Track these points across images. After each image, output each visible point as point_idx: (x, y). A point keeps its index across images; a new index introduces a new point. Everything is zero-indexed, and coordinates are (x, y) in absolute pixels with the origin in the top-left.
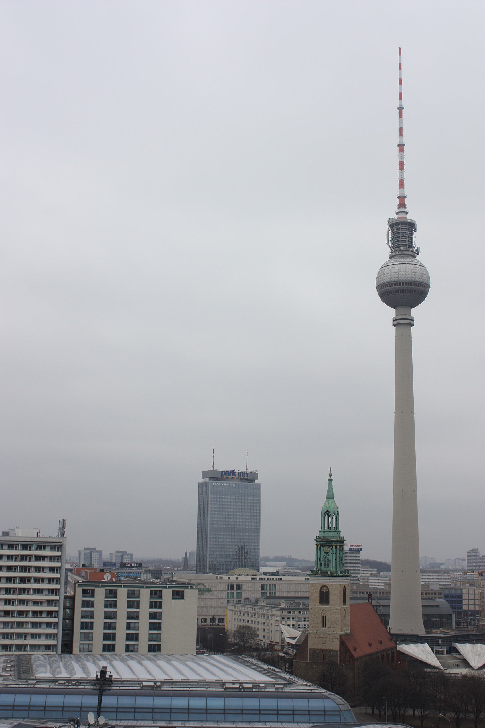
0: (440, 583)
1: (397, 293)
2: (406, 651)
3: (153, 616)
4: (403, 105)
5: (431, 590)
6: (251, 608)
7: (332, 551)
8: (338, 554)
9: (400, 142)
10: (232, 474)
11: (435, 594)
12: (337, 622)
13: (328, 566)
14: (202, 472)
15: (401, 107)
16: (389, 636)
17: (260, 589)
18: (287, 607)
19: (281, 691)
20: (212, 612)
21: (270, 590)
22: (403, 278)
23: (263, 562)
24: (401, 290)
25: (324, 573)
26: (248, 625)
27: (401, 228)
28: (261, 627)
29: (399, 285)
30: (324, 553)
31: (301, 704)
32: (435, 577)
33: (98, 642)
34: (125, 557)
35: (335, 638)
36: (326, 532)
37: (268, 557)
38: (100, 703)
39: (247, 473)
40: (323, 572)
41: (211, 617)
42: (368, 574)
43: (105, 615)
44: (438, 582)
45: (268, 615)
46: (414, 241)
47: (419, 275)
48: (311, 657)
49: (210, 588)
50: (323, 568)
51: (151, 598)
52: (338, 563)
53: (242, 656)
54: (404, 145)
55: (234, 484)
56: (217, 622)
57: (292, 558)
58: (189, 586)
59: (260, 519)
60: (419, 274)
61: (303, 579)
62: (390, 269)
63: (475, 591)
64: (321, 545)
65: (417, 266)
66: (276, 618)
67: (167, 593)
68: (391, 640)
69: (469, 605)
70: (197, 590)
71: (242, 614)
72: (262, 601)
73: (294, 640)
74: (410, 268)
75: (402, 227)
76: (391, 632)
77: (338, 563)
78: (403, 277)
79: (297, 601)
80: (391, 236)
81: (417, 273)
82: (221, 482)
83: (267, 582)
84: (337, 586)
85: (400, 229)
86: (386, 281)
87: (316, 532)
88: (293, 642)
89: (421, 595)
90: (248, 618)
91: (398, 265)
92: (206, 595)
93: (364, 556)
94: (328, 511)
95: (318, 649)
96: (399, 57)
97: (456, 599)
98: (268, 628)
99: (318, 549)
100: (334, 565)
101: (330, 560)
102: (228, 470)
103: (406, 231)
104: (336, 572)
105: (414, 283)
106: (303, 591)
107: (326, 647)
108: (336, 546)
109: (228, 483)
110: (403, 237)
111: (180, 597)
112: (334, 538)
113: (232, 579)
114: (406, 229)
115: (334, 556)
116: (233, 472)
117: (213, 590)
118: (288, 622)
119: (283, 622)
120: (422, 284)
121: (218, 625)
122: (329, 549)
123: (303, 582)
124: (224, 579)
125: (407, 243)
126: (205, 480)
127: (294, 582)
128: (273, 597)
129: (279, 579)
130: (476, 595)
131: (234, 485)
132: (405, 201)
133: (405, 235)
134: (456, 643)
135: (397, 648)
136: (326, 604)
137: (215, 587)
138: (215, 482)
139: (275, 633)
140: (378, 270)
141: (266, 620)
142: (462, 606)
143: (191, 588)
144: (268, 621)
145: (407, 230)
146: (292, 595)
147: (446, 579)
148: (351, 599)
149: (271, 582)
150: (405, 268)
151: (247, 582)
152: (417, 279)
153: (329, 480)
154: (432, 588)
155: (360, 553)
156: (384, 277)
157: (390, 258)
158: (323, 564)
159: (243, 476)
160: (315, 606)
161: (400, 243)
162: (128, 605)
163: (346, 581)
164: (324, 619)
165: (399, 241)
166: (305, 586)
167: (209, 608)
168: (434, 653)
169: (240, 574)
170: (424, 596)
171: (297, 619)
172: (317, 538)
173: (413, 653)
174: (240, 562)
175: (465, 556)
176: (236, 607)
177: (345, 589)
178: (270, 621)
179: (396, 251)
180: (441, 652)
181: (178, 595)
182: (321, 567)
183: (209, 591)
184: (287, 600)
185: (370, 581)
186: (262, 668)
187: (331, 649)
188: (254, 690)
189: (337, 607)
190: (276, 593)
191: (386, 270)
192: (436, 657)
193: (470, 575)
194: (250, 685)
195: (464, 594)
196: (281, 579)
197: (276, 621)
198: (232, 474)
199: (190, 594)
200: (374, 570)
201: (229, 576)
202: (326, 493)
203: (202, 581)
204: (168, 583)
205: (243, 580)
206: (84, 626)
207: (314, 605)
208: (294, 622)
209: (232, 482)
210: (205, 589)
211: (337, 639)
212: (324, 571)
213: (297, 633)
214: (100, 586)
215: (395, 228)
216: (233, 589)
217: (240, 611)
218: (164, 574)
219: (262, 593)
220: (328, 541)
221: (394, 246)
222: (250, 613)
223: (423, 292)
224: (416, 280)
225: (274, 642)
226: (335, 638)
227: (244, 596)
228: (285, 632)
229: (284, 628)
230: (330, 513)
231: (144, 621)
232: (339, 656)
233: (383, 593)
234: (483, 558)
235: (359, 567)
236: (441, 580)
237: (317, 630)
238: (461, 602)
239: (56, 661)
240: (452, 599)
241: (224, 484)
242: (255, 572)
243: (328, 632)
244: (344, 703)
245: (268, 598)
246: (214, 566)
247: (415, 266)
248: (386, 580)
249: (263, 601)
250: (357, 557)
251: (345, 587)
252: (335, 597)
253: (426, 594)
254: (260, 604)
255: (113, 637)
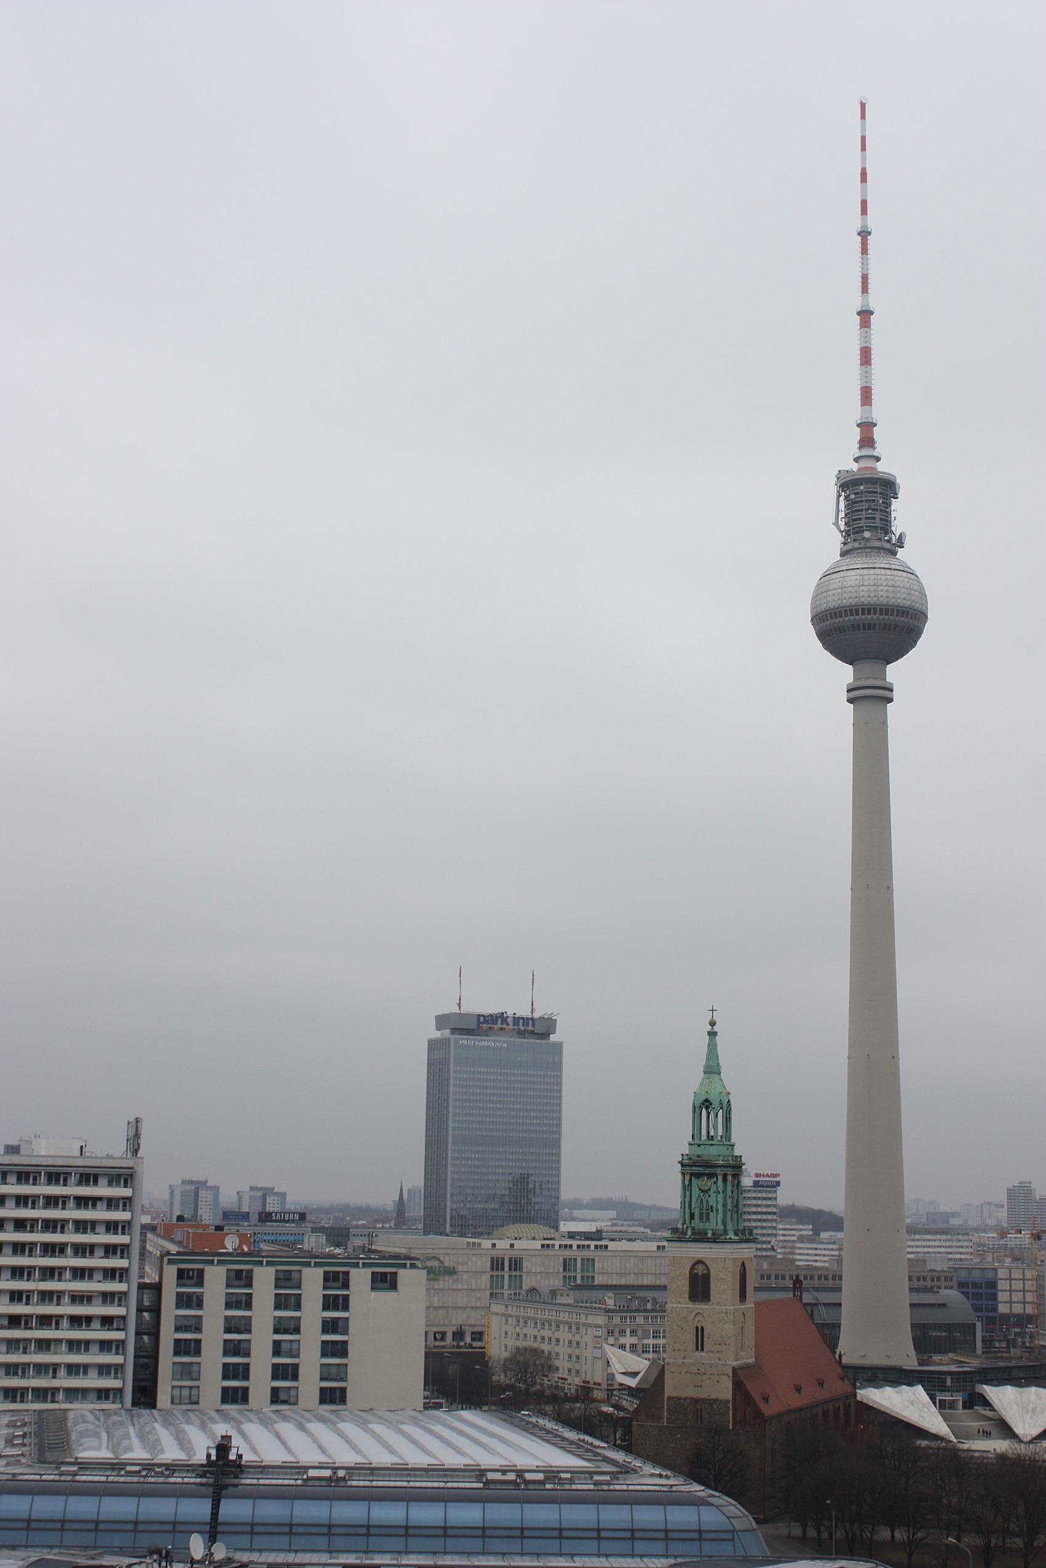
0: (950, 1256)
1: (856, 632)
2: (876, 1402)
3: (329, 1326)
4: (869, 225)
5: (931, 1270)
6: (541, 1309)
7: (717, 1188)
8: (729, 1193)
9: (862, 307)
10: (499, 1020)
11: (939, 1279)
12: (726, 1339)
13: (708, 1219)
14: (436, 1016)
15: (864, 231)
16: (840, 1371)
17: (561, 1269)
18: (620, 1307)
19: (605, 1487)
20: (457, 1319)
21: (582, 1270)
22: (869, 599)
23: (566, 1210)
24: (864, 625)
25: (699, 1234)
26: (535, 1345)
27: (866, 492)
28: (563, 1350)
29: (860, 613)
30: (698, 1192)
31: (648, 1516)
32: (937, 1243)
33: (212, 1382)
34: (269, 1200)
35: (723, 1374)
36: (704, 1146)
37: (579, 1200)
38: (215, 1514)
39: (532, 1019)
40: (696, 1231)
41: (454, 1329)
42: (794, 1235)
43: (227, 1325)
44: (946, 1253)
45: (577, 1324)
46: (893, 518)
47: (904, 593)
48: (670, 1415)
49: (454, 1267)
50: (697, 1223)
51: (325, 1288)
52: (729, 1214)
53: (522, 1412)
54: (872, 313)
55: (504, 1042)
56: (468, 1339)
57: (630, 1201)
58: (408, 1262)
59: (560, 1118)
60: (904, 590)
61: (653, 1246)
62: (841, 579)
63: (1024, 1272)
64: (692, 1175)
65: (900, 573)
66: (596, 1331)
67: (360, 1278)
68: (842, 1379)
69: (1011, 1302)
70: (426, 1271)
71: (522, 1323)
72: (565, 1295)
73: (634, 1378)
74: (884, 577)
75: (867, 488)
76: (844, 1361)
77: (729, 1214)
78: (869, 596)
79: (640, 1294)
80: (843, 509)
81: (899, 589)
82: (477, 1037)
83: (577, 1253)
84: (727, 1261)
85: (862, 493)
86: (832, 605)
87: (681, 1145)
88: (632, 1382)
89: (908, 1282)
90: (534, 1332)
91: (859, 570)
92: (445, 1282)
93: (784, 1197)
94: (707, 1100)
95: (685, 1399)
96: (862, 123)
97: (983, 1291)
98: (577, 1352)
99: (687, 1182)
100: (720, 1217)
101: (712, 1207)
102: (491, 1012)
103: (876, 497)
104: (725, 1232)
105: (894, 610)
106: (653, 1272)
107: (702, 1394)
108: (725, 1176)
109: (491, 1041)
110: (870, 511)
111: (388, 1287)
112: (721, 1158)
113: (500, 1248)
114: (876, 493)
115: (720, 1197)
116: (502, 1017)
117: (460, 1270)
118: (622, 1340)
119: (611, 1340)
120: (911, 611)
121: (470, 1347)
122: (710, 1183)
123: (654, 1254)
124: (482, 1247)
125: (878, 523)
126: (442, 1034)
127: (635, 1254)
128: (589, 1286)
129: (601, 1246)
130: (1026, 1282)
131: (506, 1045)
132: (872, 432)
133: (874, 505)
134: (984, 1384)
135: (855, 1395)
136: (702, 1302)
137: (463, 1264)
138: (464, 1039)
139: (593, 1364)
140: (816, 582)
141: (574, 1335)
142: (996, 1305)
143: (413, 1266)
144: (577, 1338)
145: (879, 495)
146: (631, 1280)
147: (962, 1247)
148: (757, 1291)
149: (585, 1253)
150: (873, 577)
151: (532, 1253)
152: (899, 601)
153: (709, 1033)
154: (931, 1265)
155: (776, 1191)
156: (829, 596)
157: (841, 556)
158: (697, 1216)
159: (523, 1025)
160: (679, 1305)
161: (862, 523)
162: (275, 1303)
163: (746, 1252)
164: (700, 1333)
165: (860, 519)
166: (658, 1261)
167: (450, 1309)
168: (936, 1407)
169: (517, 1236)
170: (915, 1284)
171: (640, 1333)
172: (683, 1160)
173: (892, 1407)
174: (517, 1210)
175: (1003, 1198)
176: (510, 1307)
177: (745, 1268)
178: (582, 1337)
179: (855, 540)
180: (952, 1405)
181: (385, 1282)
182: (692, 1221)
183: (451, 1272)
184: (618, 1292)
185: (797, 1251)
186: (564, 1439)
187: (715, 1398)
188: (548, 1486)
189: (726, 1307)
190: (596, 1277)
191: (832, 582)
192: (941, 1415)
193: (1014, 1239)
194: (540, 1476)
195: (1001, 1279)
196: (606, 1247)
197: (596, 1337)
198: (499, 1020)
199: (410, 1279)
200: (807, 1227)
201: (494, 1241)
202: (703, 1061)
203: (436, 1251)
204: (363, 1256)
205: (525, 1250)
206: (181, 1348)
207: (678, 1303)
208: (634, 1340)
209: (500, 1039)
210: (442, 1269)
211: (726, 1376)
212: (699, 1229)
213: (641, 1364)
214: (216, 1263)
215: (852, 490)
216: (503, 1269)
217: (517, 1317)
218: (354, 1235)
219: (565, 1277)
220: (708, 1164)
221: (849, 530)
222: (538, 1321)
223: (911, 629)
224: (896, 604)
225: (591, 1383)
226: (723, 1374)
227: (527, 1283)
228: (614, 1361)
229: (612, 1353)
230: (711, 1104)
231: (311, 1338)
232: (731, 1412)
233: (826, 1278)
234: (1042, 1201)
235: (775, 1220)
236: (950, 1250)
237: (684, 1358)
238: (994, 1297)
239: (121, 1423)
240: (976, 1290)
241: (484, 1042)
242: (550, 1232)
243: (708, 1362)
244: (741, 1515)
245: (579, 1287)
246: (462, 1219)
247: (896, 573)
248: (832, 1250)
249: (568, 1295)
250: (770, 1199)
251: (743, 1264)
252: (723, 1286)
253: (918, 1279)
254: (560, 1302)
255: (243, 1372)
